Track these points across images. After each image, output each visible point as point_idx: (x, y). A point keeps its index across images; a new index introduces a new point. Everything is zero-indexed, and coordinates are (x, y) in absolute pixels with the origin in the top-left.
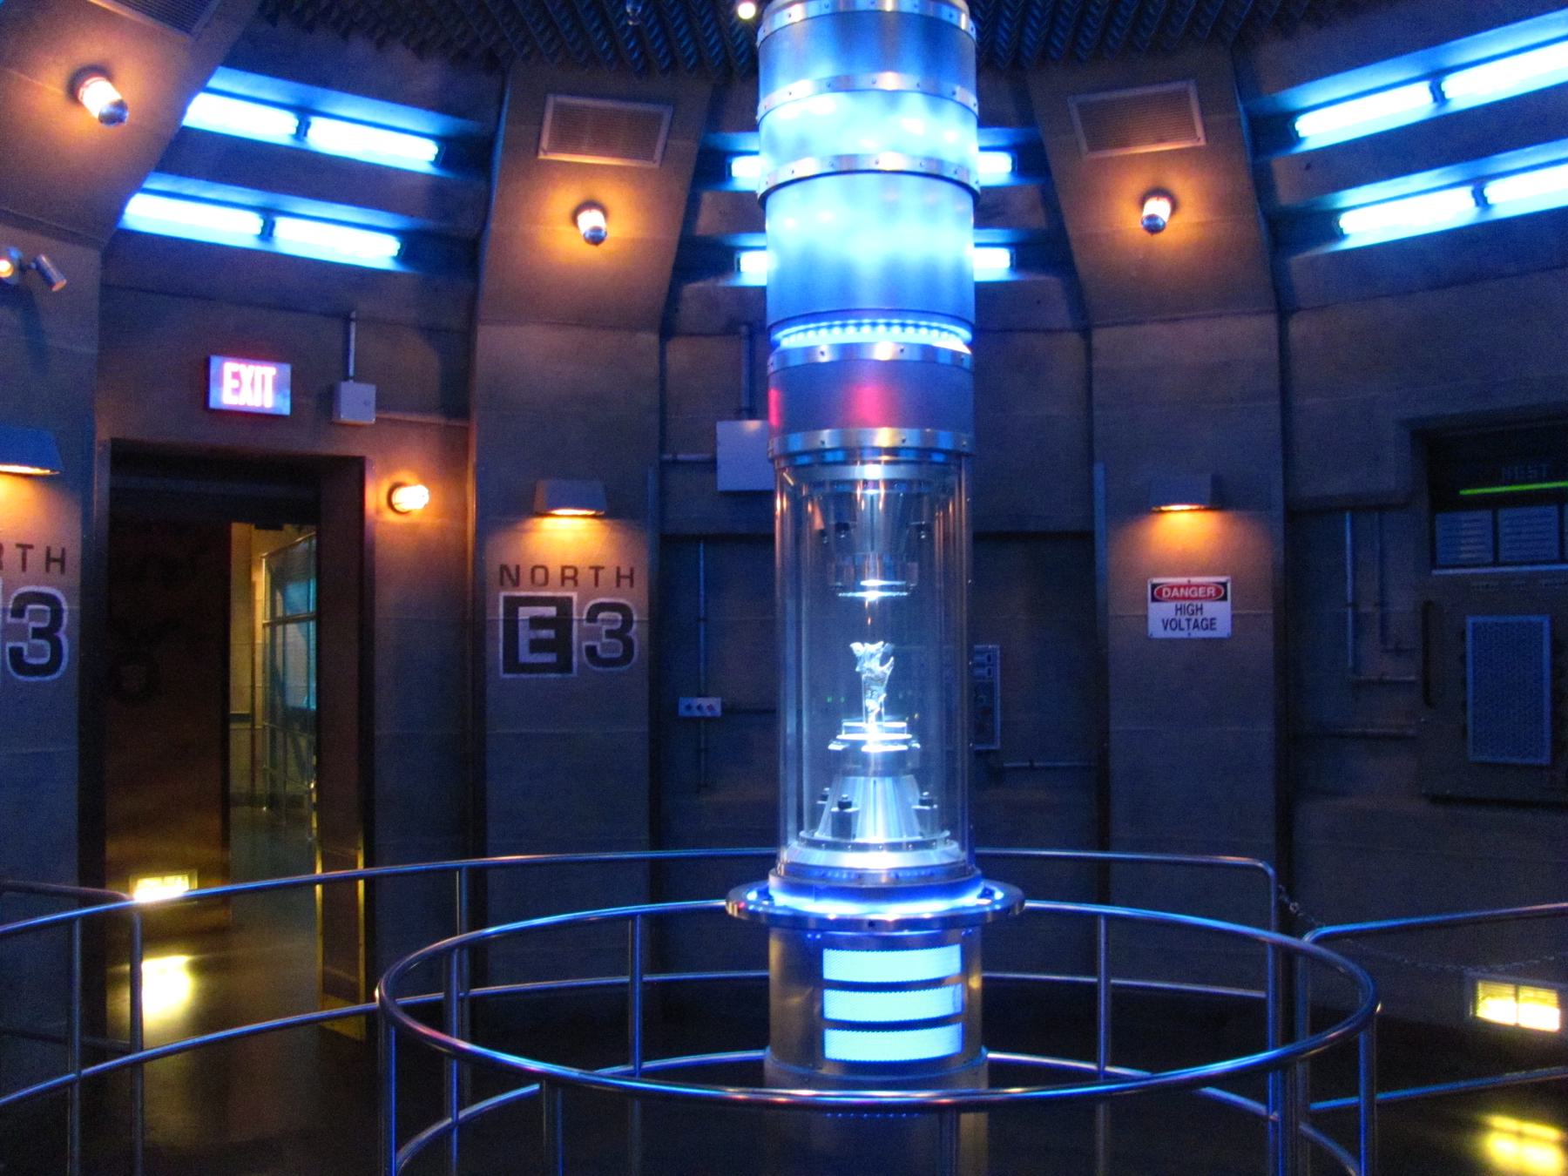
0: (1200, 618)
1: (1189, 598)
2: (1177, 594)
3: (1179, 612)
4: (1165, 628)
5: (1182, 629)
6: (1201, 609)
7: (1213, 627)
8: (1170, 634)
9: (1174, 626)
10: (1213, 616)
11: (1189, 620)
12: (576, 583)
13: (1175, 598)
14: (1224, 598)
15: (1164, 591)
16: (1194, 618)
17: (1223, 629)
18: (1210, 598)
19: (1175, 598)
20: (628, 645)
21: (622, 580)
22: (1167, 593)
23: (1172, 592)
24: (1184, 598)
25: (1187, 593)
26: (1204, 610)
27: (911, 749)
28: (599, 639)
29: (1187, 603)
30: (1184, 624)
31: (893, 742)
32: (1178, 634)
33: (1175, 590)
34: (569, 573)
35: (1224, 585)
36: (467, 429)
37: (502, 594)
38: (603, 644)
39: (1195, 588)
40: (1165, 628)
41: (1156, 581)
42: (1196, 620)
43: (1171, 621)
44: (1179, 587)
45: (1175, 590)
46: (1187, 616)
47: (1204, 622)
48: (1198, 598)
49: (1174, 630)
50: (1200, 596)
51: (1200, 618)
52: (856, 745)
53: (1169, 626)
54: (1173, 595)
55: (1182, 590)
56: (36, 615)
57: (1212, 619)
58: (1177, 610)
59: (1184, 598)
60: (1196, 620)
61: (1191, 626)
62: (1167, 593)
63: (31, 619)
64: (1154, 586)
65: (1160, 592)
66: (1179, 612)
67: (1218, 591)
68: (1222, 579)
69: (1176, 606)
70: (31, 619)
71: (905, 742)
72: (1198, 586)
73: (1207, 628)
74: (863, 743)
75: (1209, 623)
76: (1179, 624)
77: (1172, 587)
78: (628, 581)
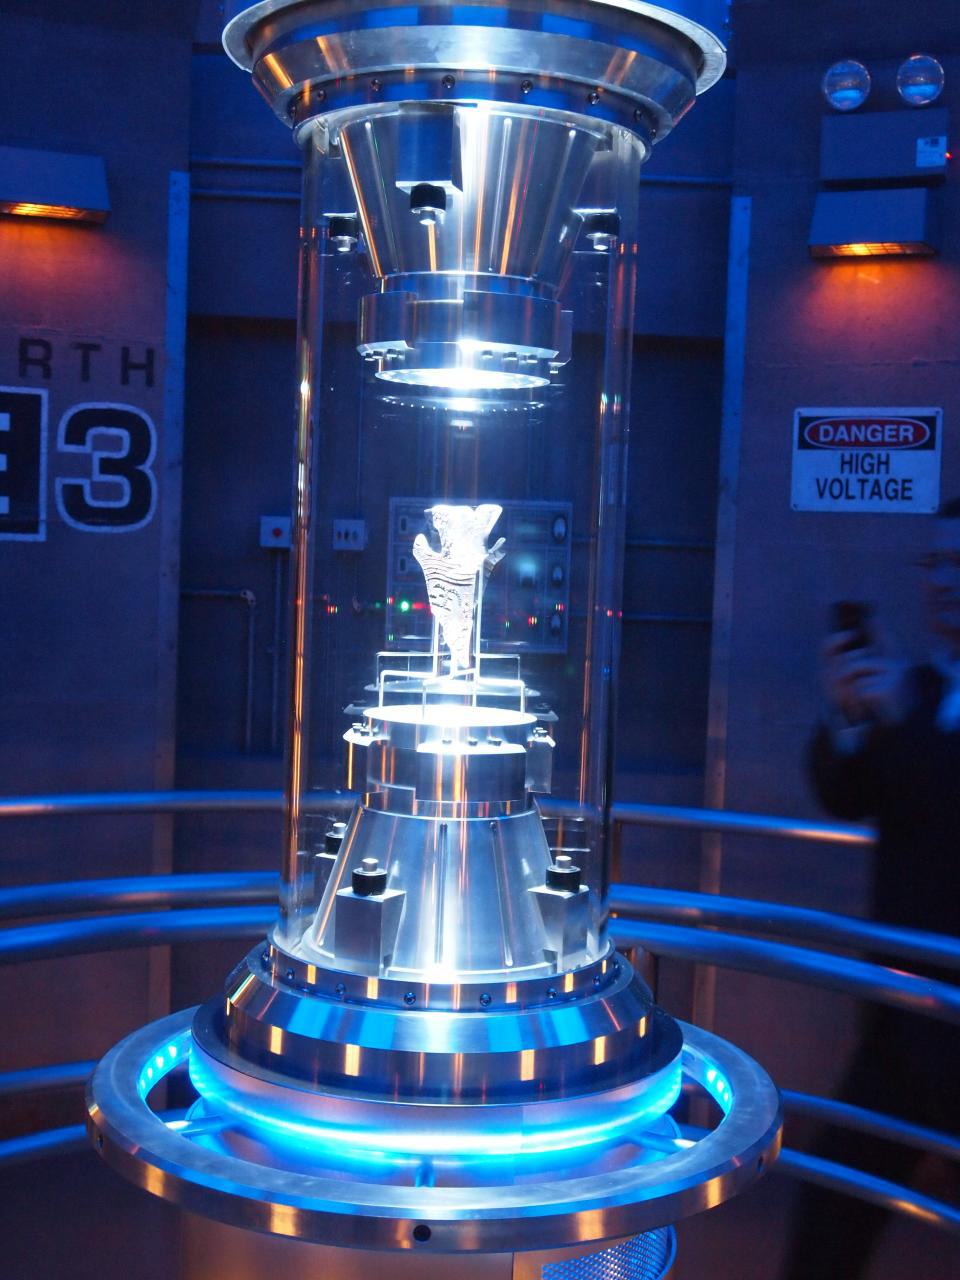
0: (883, 478)
1: (867, 444)
2: (846, 438)
3: (847, 467)
4: (821, 495)
5: (849, 497)
6: (887, 463)
7: (907, 494)
8: (826, 505)
9: (836, 492)
10: (907, 476)
11: (863, 482)
12: (47, 374)
13: (842, 443)
14: (930, 445)
15: (822, 428)
16: (872, 477)
17: (925, 499)
18: (904, 444)
19: (842, 443)
20: (141, 486)
21: (132, 373)
22: (827, 433)
23: (866, 437)
24: (857, 443)
25: (862, 434)
26: (891, 466)
27: (536, 750)
28: (88, 474)
29: (862, 452)
30: (854, 489)
31: (482, 733)
32: (843, 505)
33: (842, 428)
34: (37, 352)
35: (930, 421)
36: (297, 202)
37: (44, 394)
38: (93, 485)
39: (878, 428)
40: (821, 495)
41: (806, 412)
42: (877, 483)
43: (833, 482)
44: (848, 424)
45: (842, 428)
46: (861, 475)
47: (892, 486)
48: (883, 444)
49: (836, 498)
50: (887, 439)
51: (883, 478)
52: (402, 733)
53: (827, 493)
54: (837, 439)
55: (854, 429)
56: (102, 443)
57: (904, 481)
58: (843, 463)
59: (857, 443)
60: (877, 483)
61: (868, 492)
62: (827, 433)
63: (96, 448)
64: (805, 421)
65: (814, 433)
66: (847, 467)
67: (919, 433)
68: (926, 412)
69: (843, 456)
70: (96, 448)
71: (514, 734)
72: (883, 423)
73: (896, 497)
74: (425, 732)
75: (899, 487)
76: (845, 487)
77: (836, 424)
78: (142, 373)
